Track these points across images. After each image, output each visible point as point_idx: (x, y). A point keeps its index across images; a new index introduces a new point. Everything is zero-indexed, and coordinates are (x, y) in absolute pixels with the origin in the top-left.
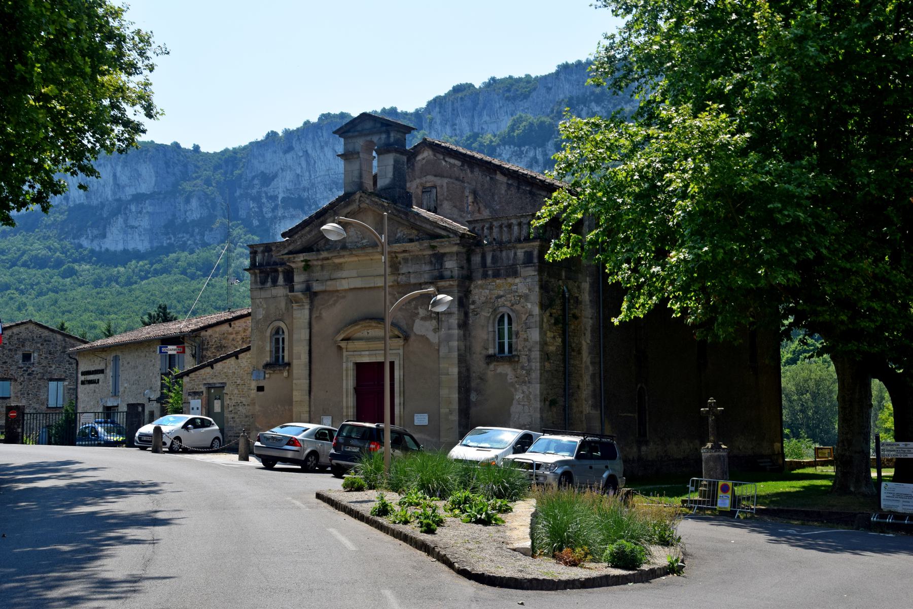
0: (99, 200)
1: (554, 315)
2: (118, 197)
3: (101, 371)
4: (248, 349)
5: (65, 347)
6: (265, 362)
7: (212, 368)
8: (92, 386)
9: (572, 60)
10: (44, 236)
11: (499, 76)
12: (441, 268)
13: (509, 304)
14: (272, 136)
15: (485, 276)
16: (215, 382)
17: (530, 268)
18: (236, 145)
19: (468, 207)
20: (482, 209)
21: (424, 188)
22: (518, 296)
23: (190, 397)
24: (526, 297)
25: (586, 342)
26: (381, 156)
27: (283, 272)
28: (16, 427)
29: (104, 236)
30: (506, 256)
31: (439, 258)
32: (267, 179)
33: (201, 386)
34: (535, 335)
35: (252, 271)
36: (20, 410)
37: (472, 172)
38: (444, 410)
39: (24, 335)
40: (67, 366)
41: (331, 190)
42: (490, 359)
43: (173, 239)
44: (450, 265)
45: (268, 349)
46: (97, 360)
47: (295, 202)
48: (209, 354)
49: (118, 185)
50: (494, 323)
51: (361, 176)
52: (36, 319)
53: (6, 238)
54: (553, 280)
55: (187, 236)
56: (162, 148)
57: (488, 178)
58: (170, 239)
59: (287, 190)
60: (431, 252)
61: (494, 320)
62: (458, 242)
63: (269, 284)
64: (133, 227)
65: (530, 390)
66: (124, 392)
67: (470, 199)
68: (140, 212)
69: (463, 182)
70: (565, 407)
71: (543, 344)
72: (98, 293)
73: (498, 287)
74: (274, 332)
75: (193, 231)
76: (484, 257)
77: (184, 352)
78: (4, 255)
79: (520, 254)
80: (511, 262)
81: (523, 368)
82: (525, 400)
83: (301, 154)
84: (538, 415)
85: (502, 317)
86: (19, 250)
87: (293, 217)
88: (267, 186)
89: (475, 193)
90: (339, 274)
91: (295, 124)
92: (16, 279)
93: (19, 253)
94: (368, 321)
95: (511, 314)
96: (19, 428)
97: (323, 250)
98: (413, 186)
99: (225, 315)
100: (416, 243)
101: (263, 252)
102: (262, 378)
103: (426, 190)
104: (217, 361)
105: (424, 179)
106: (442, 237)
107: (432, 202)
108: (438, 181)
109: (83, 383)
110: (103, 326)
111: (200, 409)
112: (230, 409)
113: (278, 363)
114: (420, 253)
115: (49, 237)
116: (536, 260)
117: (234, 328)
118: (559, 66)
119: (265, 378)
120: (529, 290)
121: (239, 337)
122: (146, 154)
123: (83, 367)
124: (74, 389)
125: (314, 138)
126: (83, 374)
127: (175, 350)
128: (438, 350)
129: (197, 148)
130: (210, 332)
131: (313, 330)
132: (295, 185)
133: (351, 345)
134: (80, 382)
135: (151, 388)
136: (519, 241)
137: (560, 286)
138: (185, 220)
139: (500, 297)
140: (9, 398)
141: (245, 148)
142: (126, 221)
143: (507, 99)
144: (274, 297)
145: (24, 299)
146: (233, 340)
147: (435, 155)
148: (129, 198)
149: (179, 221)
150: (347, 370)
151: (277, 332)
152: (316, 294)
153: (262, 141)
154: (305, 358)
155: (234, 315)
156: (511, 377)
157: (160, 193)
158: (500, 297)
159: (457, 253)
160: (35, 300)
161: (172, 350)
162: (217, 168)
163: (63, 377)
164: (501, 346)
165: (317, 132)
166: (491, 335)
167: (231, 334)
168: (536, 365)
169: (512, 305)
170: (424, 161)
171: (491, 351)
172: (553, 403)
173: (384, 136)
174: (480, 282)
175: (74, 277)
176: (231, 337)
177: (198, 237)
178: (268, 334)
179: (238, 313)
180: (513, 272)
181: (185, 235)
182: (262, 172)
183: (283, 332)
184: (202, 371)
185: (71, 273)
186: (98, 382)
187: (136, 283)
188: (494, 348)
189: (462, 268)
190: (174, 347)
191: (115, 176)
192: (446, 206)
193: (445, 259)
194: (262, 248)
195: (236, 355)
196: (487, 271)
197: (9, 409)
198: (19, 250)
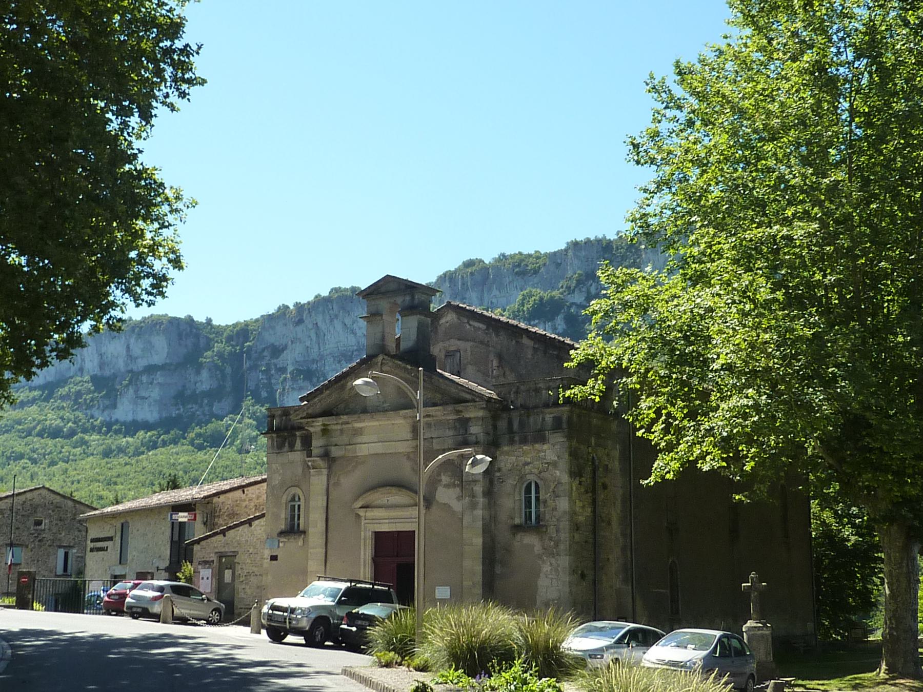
0: (112, 371)
1: (583, 483)
2: (129, 368)
3: (110, 539)
4: (263, 515)
5: (75, 515)
6: (279, 530)
7: (224, 536)
8: (101, 553)
9: (581, 238)
10: (58, 407)
11: (508, 253)
12: (466, 433)
13: (536, 471)
14: (283, 310)
15: (512, 442)
16: (227, 550)
17: (559, 434)
18: (248, 319)
19: (492, 372)
20: (508, 373)
21: (448, 352)
22: (546, 463)
23: (200, 567)
24: (555, 464)
25: (615, 513)
26: (404, 318)
27: (301, 437)
28: (26, 592)
29: (114, 406)
30: (534, 421)
31: (464, 423)
32: (277, 351)
33: (212, 555)
34: (563, 504)
35: (269, 435)
36: (31, 576)
37: (497, 335)
38: (467, 583)
39: (37, 501)
40: (76, 533)
41: (339, 362)
42: (517, 529)
43: (182, 410)
44: (475, 430)
45: (283, 516)
46: (107, 527)
47: (306, 373)
48: (221, 521)
49: (131, 356)
50: (520, 491)
51: (383, 339)
52: (47, 486)
53: (23, 409)
54: (582, 447)
55: (195, 407)
56: (174, 321)
57: (514, 341)
58: (179, 409)
59: (297, 362)
60: (455, 417)
61: (521, 489)
62: (484, 406)
63: (286, 448)
64: (143, 398)
65: (559, 562)
66: (133, 559)
67: (495, 363)
68: (151, 383)
69: (488, 346)
70: (595, 581)
71: (573, 514)
72: (107, 463)
73: (525, 453)
74: (289, 498)
75: (202, 401)
76: (510, 423)
77: (195, 519)
78: (20, 425)
79: (549, 418)
80: (539, 427)
81: (551, 539)
82: (553, 573)
83: (310, 326)
84: (568, 590)
85: (530, 484)
86: (34, 420)
87: (301, 389)
88: (277, 358)
89: (500, 357)
90: (359, 439)
91: (306, 297)
92: (30, 449)
93: (34, 424)
94: (388, 488)
95: (538, 481)
96: (29, 594)
97: (343, 415)
98: (437, 350)
99: (237, 482)
100: (440, 408)
101: (281, 416)
102: (276, 546)
103: (449, 354)
104: (230, 528)
105: (448, 343)
106: (467, 401)
107: (455, 366)
108: (461, 345)
109: (92, 550)
110: (112, 497)
111: (210, 579)
112: (241, 580)
113: (293, 530)
114: (443, 418)
115: (63, 408)
116: (564, 426)
117: (247, 495)
118: (568, 243)
119: (279, 546)
120: (558, 457)
121: (253, 504)
122: (160, 327)
123: (93, 534)
124: (82, 557)
125: (324, 312)
126: (93, 541)
127: (186, 517)
128: (462, 520)
129: (209, 321)
130: (222, 497)
131: (330, 497)
132: (304, 357)
133: (371, 513)
134: (89, 549)
135: (160, 557)
136: (547, 405)
137: (589, 453)
138: (195, 391)
139: (527, 464)
140: (20, 564)
141: (257, 320)
142: (136, 392)
143: (518, 274)
144: (292, 462)
145: (36, 469)
146: (246, 507)
147: (459, 319)
148: (141, 369)
149: (188, 392)
150: (365, 539)
151: (293, 499)
152: (334, 460)
153: (273, 314)
154: (321, 526)
155: (247, 482)
156: (538, 549)
157: (171, 364)
158: (527, 464)
159: (483, 419)
160: (47, 470)
161: (183, 517)
162: (229, 339)
163: (72, 544)
164: (528, 516)
165: (328, 306)
166: (517, 503)
167: (245, 500)
168: (564, 536)
169: (540, 473)
170: (448, 324)
171: (517, 521)
172: (583, 576)
173: (408, 298)
174: (506, 448)
175: (84, 447)
176: (244, 504)
177: (207, 408)
178: (284, 499)
179: (252, 480)
180: (540, 437)
181: (194, 406)
182: (273, 344)
183: (299, 499)
184: (214, 539)
185: (84, 443)
186: (107, 550)
187: (143, 453)
188: (521, 518)
189: (488, 434)
190: (186, 514)
191: (128, 347)
192: (470, 369)
193: (470, 424)
194: (280, 412)
195: (249, 522)
196: (514, 437)
197: (21, 574)
198: (34, 420)
